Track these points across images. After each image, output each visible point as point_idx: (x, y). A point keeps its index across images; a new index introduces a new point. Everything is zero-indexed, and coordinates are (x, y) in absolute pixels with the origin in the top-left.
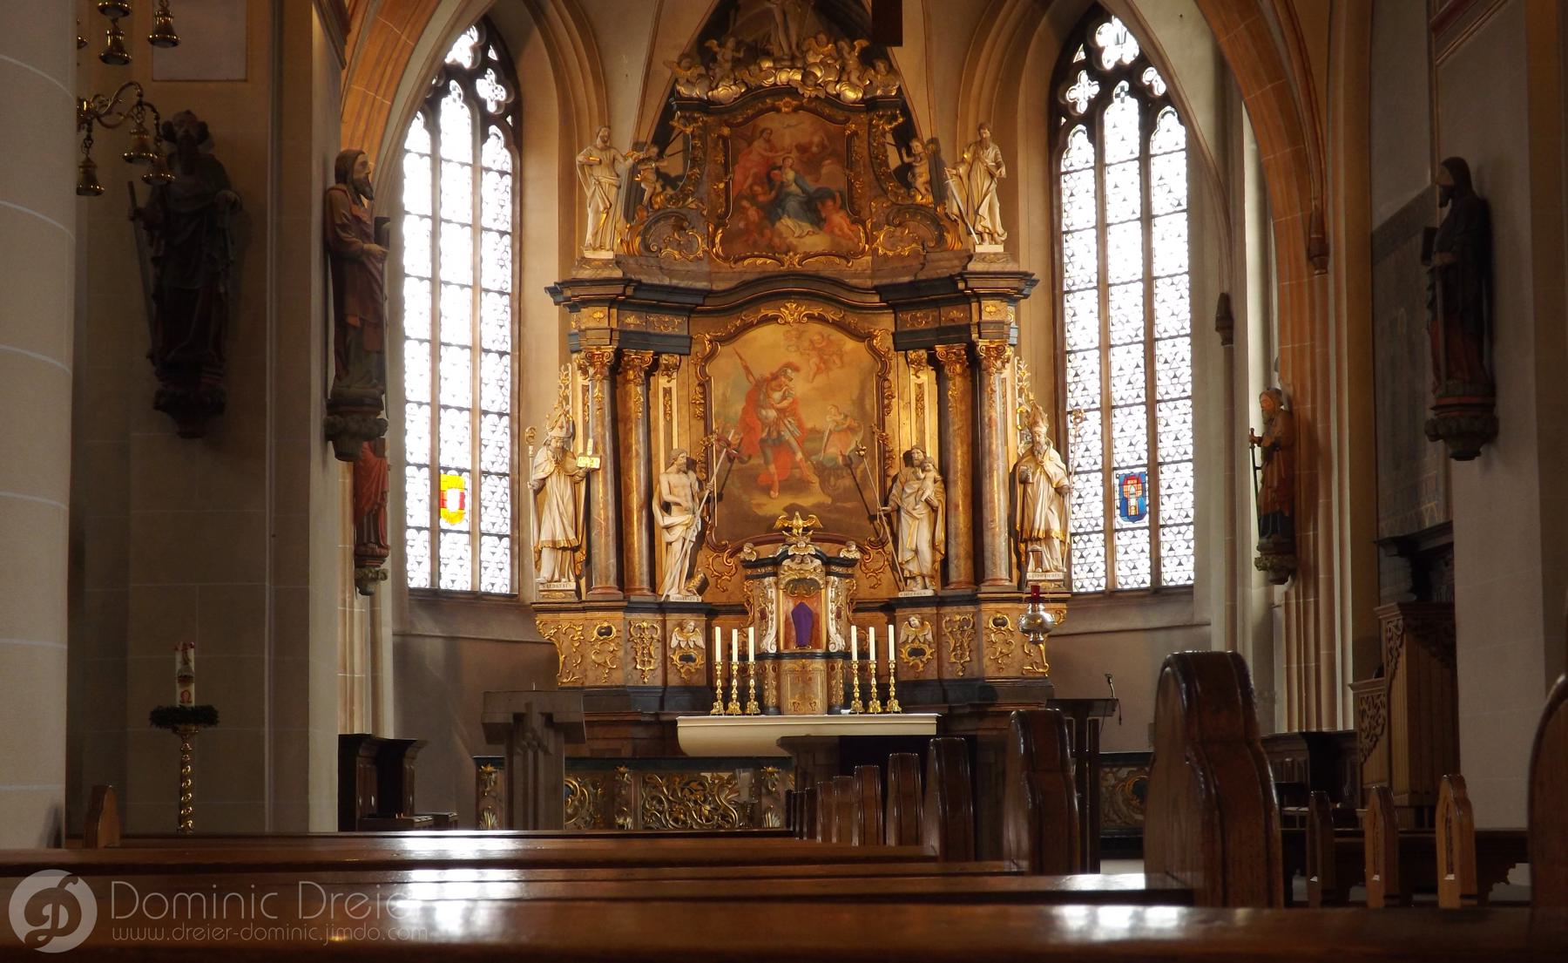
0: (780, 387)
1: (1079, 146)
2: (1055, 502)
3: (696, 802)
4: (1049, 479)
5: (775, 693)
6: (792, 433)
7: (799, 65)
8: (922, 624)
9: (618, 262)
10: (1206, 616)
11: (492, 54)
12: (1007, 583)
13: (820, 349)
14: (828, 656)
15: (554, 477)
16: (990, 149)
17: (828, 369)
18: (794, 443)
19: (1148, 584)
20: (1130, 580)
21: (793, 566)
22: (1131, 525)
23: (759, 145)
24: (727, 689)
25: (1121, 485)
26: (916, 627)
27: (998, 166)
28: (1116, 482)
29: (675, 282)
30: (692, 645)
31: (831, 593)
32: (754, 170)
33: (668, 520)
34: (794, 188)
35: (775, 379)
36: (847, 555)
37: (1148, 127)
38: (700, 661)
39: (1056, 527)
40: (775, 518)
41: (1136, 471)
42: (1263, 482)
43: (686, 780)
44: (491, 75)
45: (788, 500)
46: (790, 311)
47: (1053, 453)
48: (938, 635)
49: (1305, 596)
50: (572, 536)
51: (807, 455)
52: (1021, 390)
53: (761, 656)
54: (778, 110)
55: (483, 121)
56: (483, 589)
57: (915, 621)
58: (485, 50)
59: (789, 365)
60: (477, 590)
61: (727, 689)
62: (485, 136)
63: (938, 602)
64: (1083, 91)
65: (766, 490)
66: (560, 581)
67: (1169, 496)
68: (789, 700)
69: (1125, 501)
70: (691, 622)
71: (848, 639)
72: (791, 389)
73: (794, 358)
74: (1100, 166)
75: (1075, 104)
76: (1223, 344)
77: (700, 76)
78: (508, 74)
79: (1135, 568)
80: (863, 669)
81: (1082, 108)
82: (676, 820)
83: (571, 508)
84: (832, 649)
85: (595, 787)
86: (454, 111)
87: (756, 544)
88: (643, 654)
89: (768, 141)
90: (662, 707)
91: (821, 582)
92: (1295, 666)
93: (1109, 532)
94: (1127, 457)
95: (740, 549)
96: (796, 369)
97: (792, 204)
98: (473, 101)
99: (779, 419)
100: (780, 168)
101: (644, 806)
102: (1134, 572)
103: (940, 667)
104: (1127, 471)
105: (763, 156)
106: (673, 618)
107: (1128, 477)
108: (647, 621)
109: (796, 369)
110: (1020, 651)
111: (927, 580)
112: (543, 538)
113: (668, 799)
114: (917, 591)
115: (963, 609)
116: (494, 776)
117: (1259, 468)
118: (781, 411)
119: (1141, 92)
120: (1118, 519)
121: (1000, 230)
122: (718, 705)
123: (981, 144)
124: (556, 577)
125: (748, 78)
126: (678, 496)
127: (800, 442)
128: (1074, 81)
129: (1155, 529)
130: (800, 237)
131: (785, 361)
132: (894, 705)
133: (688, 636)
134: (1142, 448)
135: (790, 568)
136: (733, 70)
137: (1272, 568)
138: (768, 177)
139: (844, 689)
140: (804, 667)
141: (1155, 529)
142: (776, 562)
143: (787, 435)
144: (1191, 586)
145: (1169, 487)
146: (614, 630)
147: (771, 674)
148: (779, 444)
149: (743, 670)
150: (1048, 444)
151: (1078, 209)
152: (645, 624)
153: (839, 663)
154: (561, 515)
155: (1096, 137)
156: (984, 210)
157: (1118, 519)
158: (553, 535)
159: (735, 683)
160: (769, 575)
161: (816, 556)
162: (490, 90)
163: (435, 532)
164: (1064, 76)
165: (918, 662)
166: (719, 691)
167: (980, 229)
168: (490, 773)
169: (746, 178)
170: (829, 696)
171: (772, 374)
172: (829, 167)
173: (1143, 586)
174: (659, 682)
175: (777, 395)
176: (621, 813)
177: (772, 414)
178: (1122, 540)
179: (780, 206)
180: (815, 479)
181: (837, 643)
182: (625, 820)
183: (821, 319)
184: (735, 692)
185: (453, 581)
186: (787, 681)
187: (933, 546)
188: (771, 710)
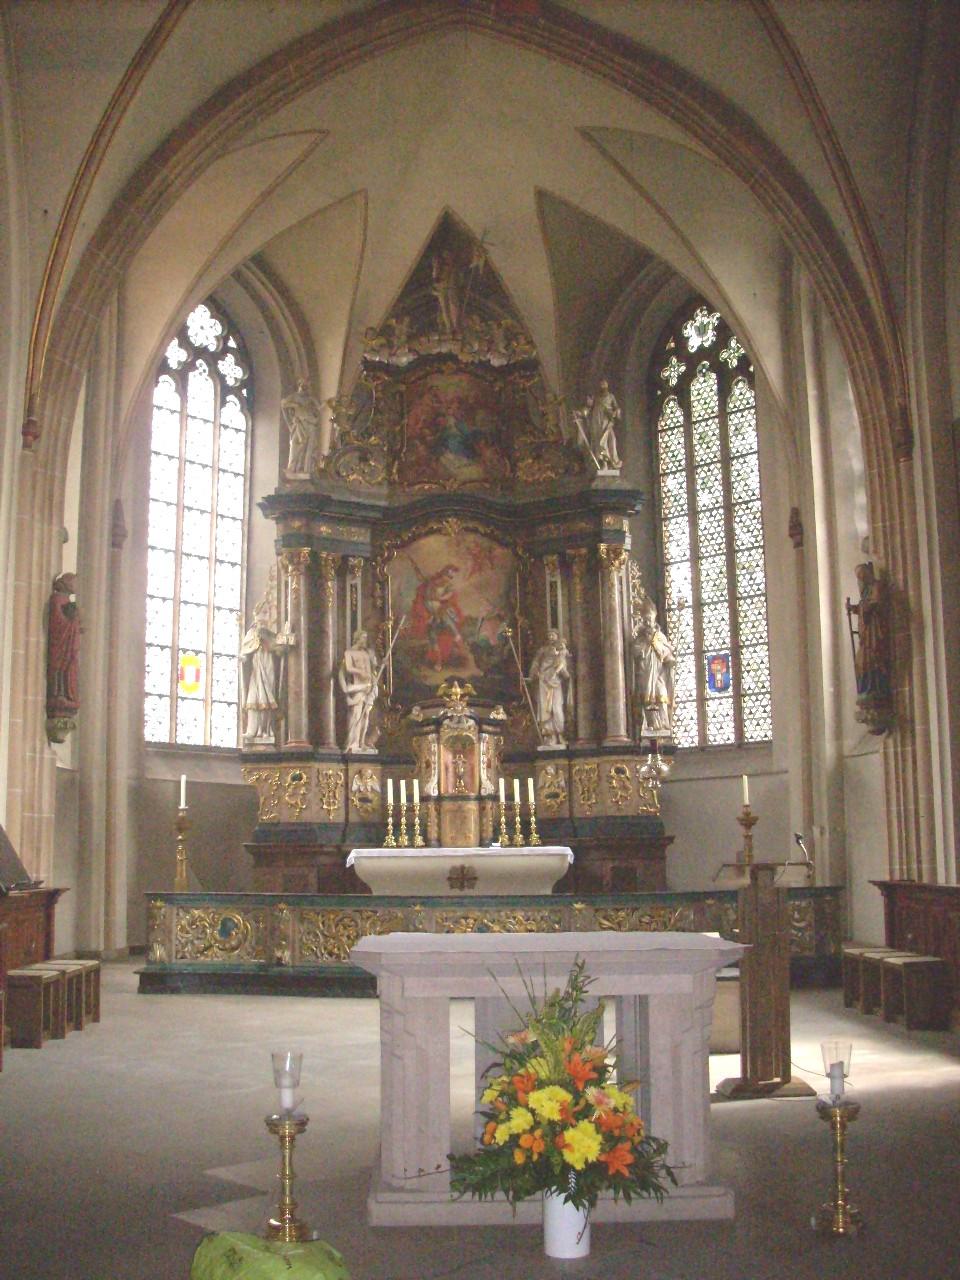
0: (442, 585)
1: (673, 412)
2: (663, 674)
3: (349, 937)
4: (658, 656)
5: (436, 828)
6: (452, 619)
7: (460, 338)
8: (557, 773)
9: (311, 481)
10: (784, 765)
11: (232, 343)
12: (626, 739)
13: (475, 555)
14: (480, 799)
15: (259, 653)
16: (608, 398)
17: (480, 569)
18: (453, 626)
19: (696, 743)
20: (718, 738)
21: (453, 725)
22: (717, 695)
23: (427, 399)
24: (397, 825)
25: (709, 664)
26: (552, 775)
27: (614, 409)
28: (706, 662)
29: (360, 500)
30: (369, 789)
31: (483, 747)
32: (423, 417)
33: (352, 688)
34: (454, 430)
35: (441, 576)
36: (496, 716)
37: (724, 392)
38: (376, 799)
39: (664, 697)
40: (438, 687)
41: (722, 653)
42: (861, 644)
43: (341, 916)
44: (230, 358)
45: (448, 674)
46: (452, 524)
47: (660, 635)
48: (570, 782)
49: (903, 745)
50: (272, 700)
51: (465, 637)
52: (634, 587)
53: (424, 799)
54: (442, 372)
55: (224, 390)
56: (179, 742)
57: (551, 770)
58: (225, 339)
59: (450, 567)
60: (208, 744)
61: (397, 825)
62: (223, 403)
63: (569, 754)
64: (673, 372)
65: (431, 665)
66: (261, 736)
67: (748, 672)
68: (448, 833)
69: (712, 676)
70: (369, 770)
71: (497, 785)
72: (451, 585)
73: (454, 561)
74: (689, 424)
75: (667, 381)
76: (795, 547)
77: (382, 346)
78: (244, 357)
79: (721, 728)
80: (510, 808)
81: (674, 382)
82: (331, 954)
83: (272, 678)
84: (483, 793)
85: (257, 922)
86: (200, 383)
87: (423, 708)
88: (329, 796)
89: (436, 396)
90: (344, 841)
91: (474, 738)
92: (894, 808)
93: (702, 701)
94: (714, 642)
95: (409, 711)
96: (456, 570)
97: (452, 443)
98: (218, 377)
99: (440, 609)
100: (444, 416)
101: (301, 940)
102: (721, 731)
103: (571, 808)
104: (714, 654)
105: (433, 408)
106: (353, 767)
107: (714, 658)
108: (332, 769)
109: (456, 570)
110: (636, 794)
111: (560, 737)
112: (249, 701)
113: (323, 934)
114: (553, 745)
115: (590, 760)
116: (163, 910)
117: (855, 632)
118: (442, 602)
119: (720, 369)
120: (708, 690)
121: (617, 459)
122: (390, 839)
123: (601, 393)
124: (259, 733)
125: (418, 347)
126: (360, 668)
127: (459, 626)
128: (667, 363)
129: (738, 696)
130: (459, 467)
131: (446, 563)
132: (535, 836)
133: (367, 781)
134: (726, 634)
135: (448, 726)
136: (407, 342)
137: (873, 721)
138: (435, 422)
139: (494, 826)
140: (460, 807)
141: (738, 696)
142: (438, 723)
143: (449, 622)
144: (770, 742)
145: (748, 665)
146: (305, 776)
147: (433, 813)
148: (442, 629)
149: (411, 809)
150: (656, 627)
151: (672, 444)
152: (331, 772)
153: (489, 804)
154: (263, 682)
155: (685, 405)
156: (603, 442)
157: (708, 690)
158: (257, 700)
159: (403, 820)
160: (432, 732)
161: (471, 717)
162: (231, 370)
163: (174, 698)
164: (660, 360)
165: (553, 803)
166: (390, 827)
167: (601, 457)
168: (160, 908)
169: (417, 423)
170: (481, 831)
171: (438, 574)
172: (481, 415)
173: (729, 742)
174: (341, 819)
175: (440, 590)
176: (280, 946)
177: (436, 605)
178: (711, 707)
179: (443, 445)
180: (471, 657)
181: (488, 788)
182: (283, 953)
183: (475, 531)
184: (403, 827)
185: (188, 738)
186: (447, 818)
187: (565, 707)
188: (433, 842)
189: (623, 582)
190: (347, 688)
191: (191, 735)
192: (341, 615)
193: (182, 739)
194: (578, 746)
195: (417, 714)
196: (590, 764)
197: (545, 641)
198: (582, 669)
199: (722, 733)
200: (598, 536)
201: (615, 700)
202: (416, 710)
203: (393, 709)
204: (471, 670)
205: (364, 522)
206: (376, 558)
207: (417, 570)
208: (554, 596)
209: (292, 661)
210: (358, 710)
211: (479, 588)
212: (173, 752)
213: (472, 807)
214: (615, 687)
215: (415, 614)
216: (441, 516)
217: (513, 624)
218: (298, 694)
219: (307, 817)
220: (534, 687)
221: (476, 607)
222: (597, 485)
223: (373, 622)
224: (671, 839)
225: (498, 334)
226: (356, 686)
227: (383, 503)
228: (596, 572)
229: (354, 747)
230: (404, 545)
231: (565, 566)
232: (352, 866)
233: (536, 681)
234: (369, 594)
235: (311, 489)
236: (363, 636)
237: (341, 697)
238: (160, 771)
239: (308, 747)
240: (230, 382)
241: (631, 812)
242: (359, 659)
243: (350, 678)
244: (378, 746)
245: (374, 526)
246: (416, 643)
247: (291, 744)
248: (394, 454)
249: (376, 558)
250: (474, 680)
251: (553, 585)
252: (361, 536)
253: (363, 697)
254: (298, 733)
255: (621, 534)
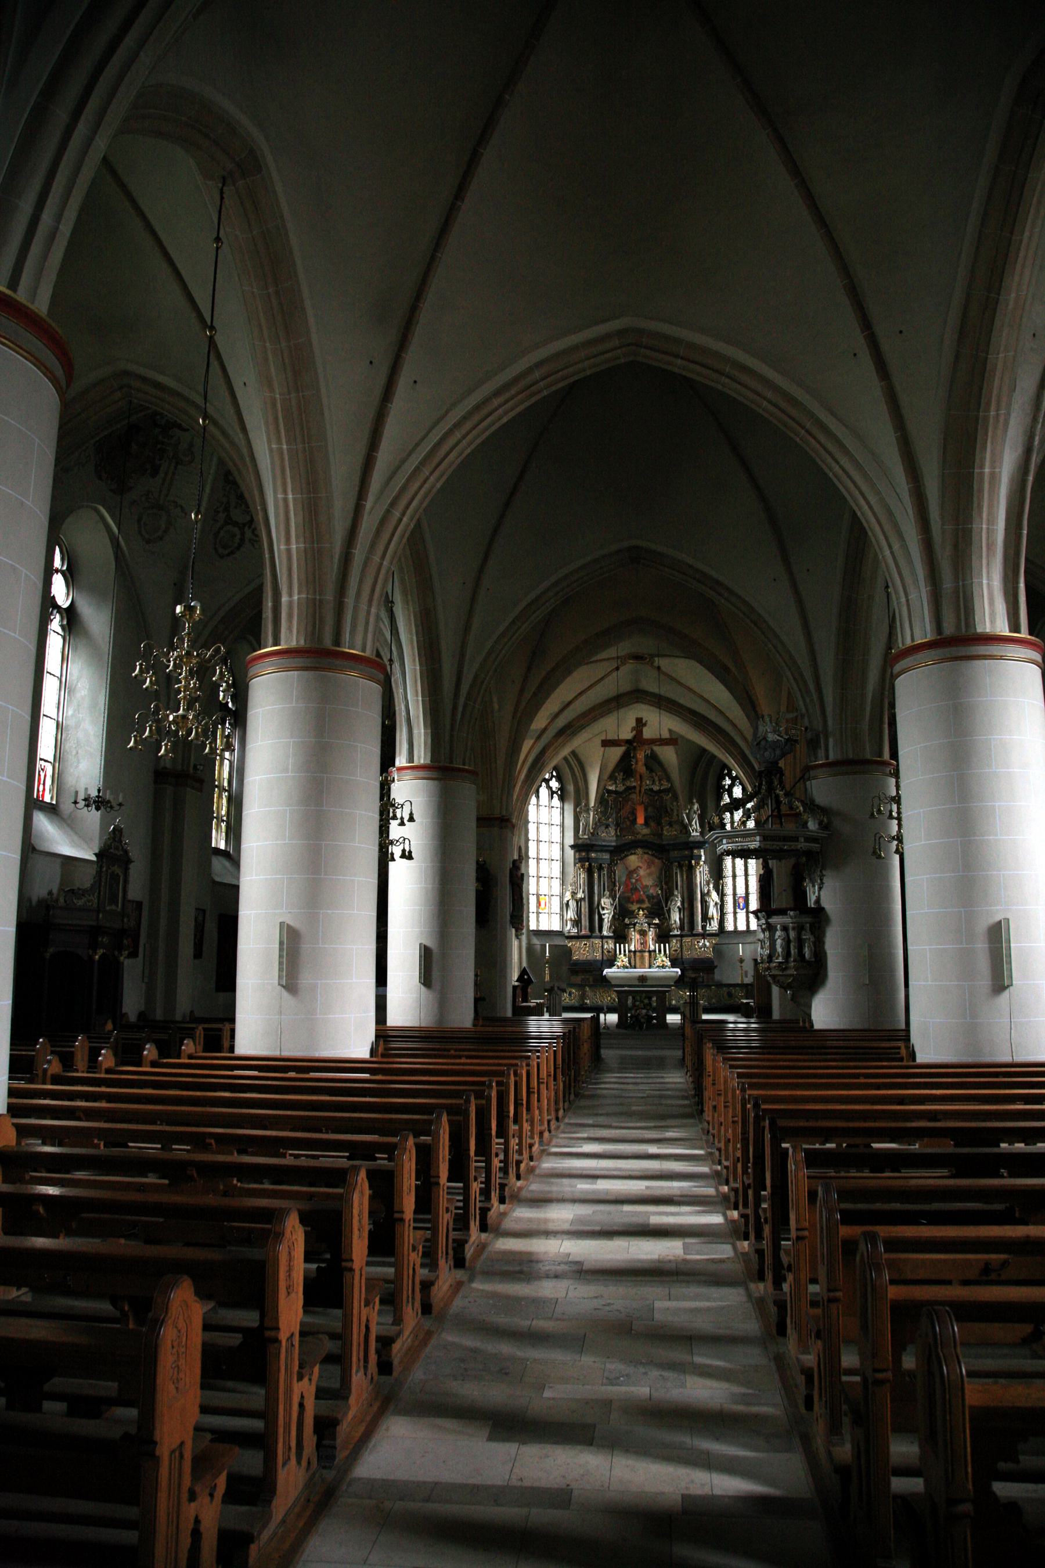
14: (650, 952)
31: (650, 933)
35: (635, 871)
45: (638, 906)
46: (640, 851)
48: (681, 946)
51: (644, 893)
53: (630, 951)
55: (552, 793)
57: (674, 941)
63: (681, 936)
64: (728, 782)
70: (610, 941)
73: (640, 864)
93: (735, 913)
98: (549, 788)
106: (604, 940)
108: (597, 941)
114: (676, 932)
128: (725, 779)
133: (610, 945)
142: (635, 925)
156: (693, 823)
177: (634, 881)
178: (738, 916)
181: (652, 948)
183: (647, 853)
187: (680, 919)
189: (702, 874)
190: (602, 912)
191: (544, 927)
192: (599, 885)
193: (541, 928)
194: (684, 933)
195: (627, 921)
196: (689, 939)
197: (673, 894)
198: (686, 905)
199: (742, 927)
200: (692, 857)
201: (697, 917)
202: (626, 920)
203: (618, 919)
204: (646, 905)
205: (606, 851)
206: (612, 863)
207: (627, 868)
208: (677, 876)
209: (583, 903)
210: (606, 920)
211: (650, 874)
212: (538, 933)
213: (647, 954)
214: (697, 912)
215: (626, 885)
216: (637, 847)
217: (661, 889)
218: (290, 616)
219: (589, 958)
220: (669, 911)
221: (648, 882)
222: (691, 839)
223: (611, 887)
224: (716, 967)
225: (656, 779)
226: (605, 911)
227: (614, 844)
228: (691, 871)
229: (605, 933)
230: (622, 859)
231: (680, 866)
232: (96, 854)
233: (670, 909)
234: (609, 877)
235: (588, 842)
236: (607, 893)
237: (600, 915)
238: (536, 941)
239: (589, 933)
240: (554, 789)
241: (702, 957)
242: (606, 902)
243: (603, 909)
244: (613, 932)
245: (611, 852)
246: (626, 895)
247: (583, 932)
248: (617, 825)
249: (612, 863)
250: (647, 908)
251: (676, 873)
252: (606, 856)
253: (608, 915)
254: (585, 929)
255: (700, 856)
